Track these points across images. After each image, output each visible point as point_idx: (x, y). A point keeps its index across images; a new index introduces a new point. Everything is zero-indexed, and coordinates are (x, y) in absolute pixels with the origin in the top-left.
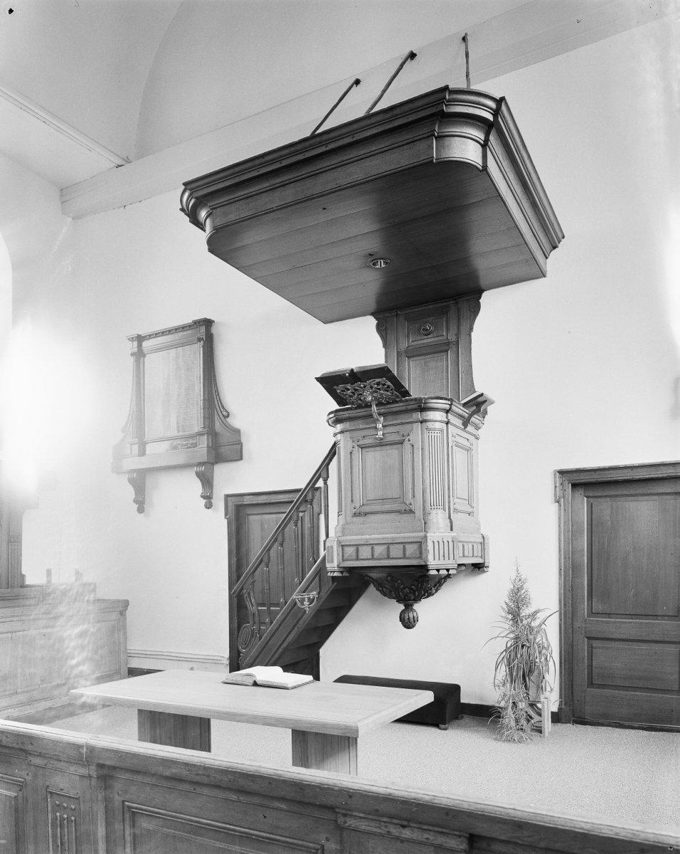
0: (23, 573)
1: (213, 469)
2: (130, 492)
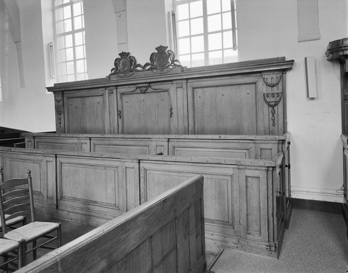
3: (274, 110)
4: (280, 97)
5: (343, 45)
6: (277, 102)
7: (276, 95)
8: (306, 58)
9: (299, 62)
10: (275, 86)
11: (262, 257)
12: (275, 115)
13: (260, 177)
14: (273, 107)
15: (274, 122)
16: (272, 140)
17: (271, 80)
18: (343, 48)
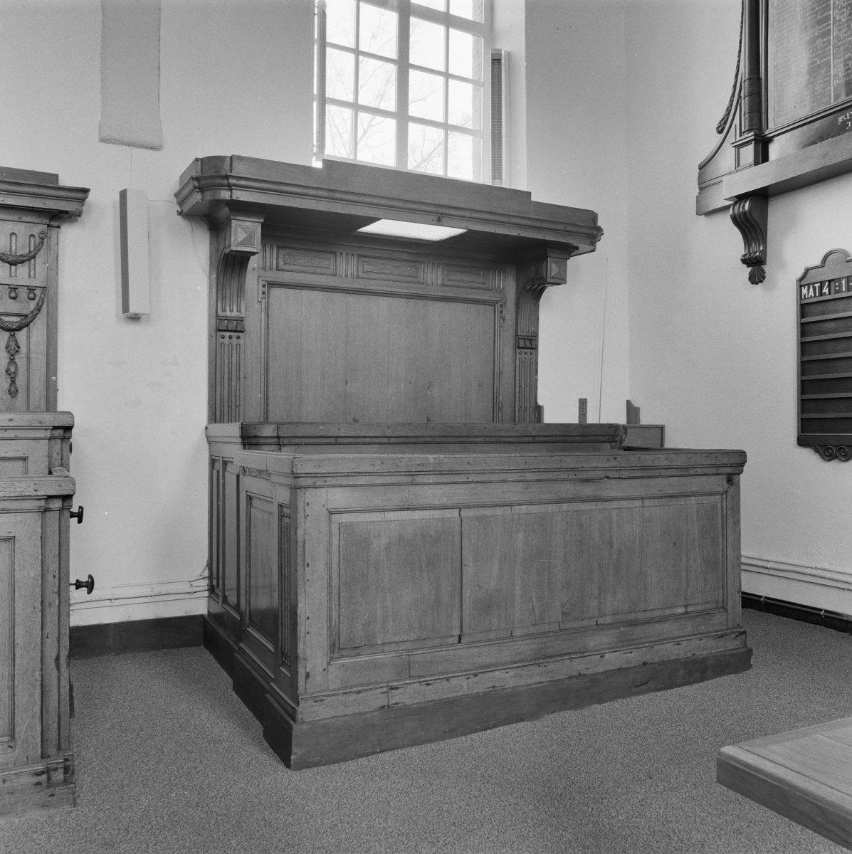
0: (540, 402)
1: (566, 264)
2: (732, 242)
3: (16, 341)
4: (37, 300)
5: (231, 172)
6: (26, 316)
7: (23, 293)
8: (123, 194)
9: (102, 200)
10: (22, 262)
11: (17, 820)
12: (20, 360)
13: (17, 538)
14: (12, 330)
15: (13, 382)
16: (31, 428)
17: (11, 240)
18: (232, 181)
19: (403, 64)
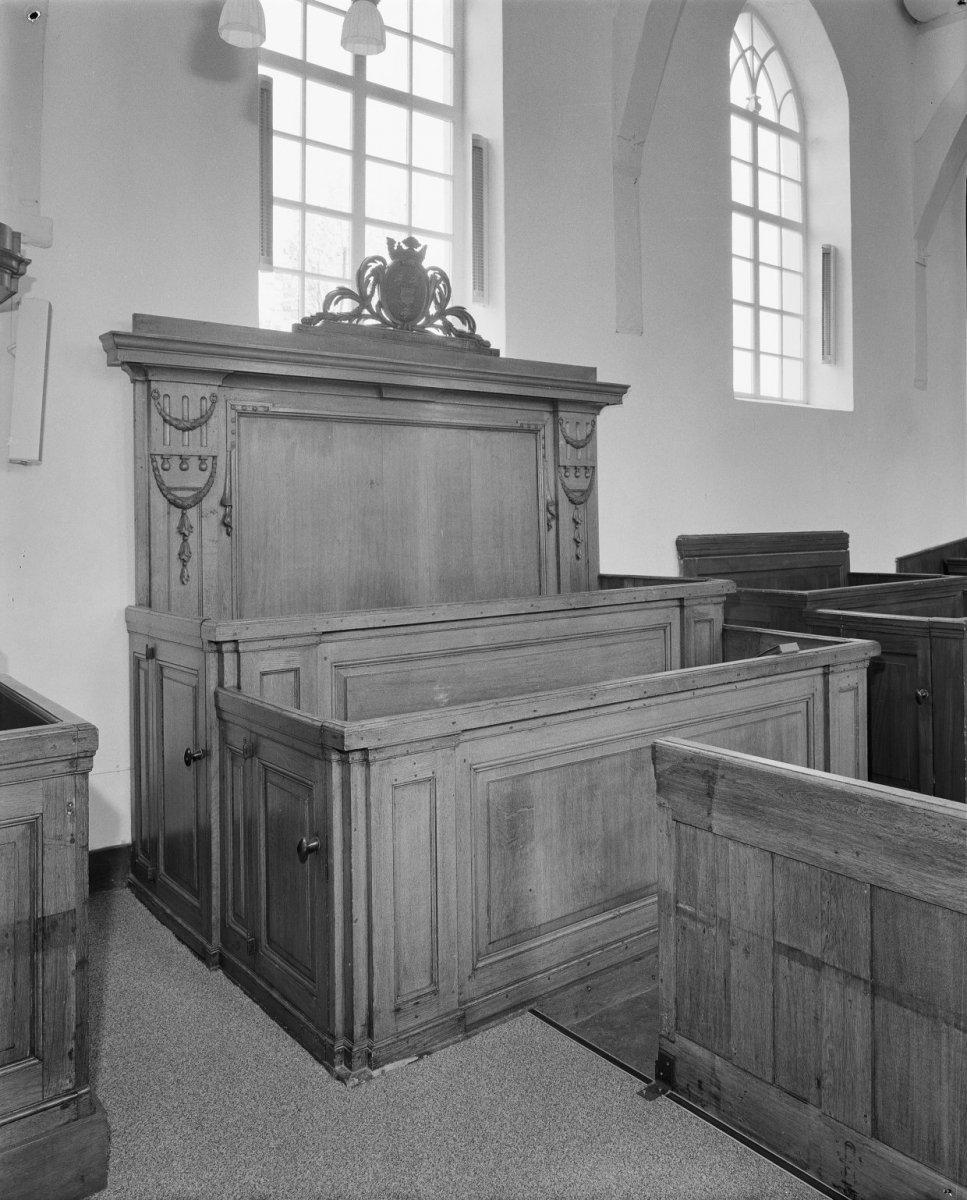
7: (194, 463)
19: (359, 154)
